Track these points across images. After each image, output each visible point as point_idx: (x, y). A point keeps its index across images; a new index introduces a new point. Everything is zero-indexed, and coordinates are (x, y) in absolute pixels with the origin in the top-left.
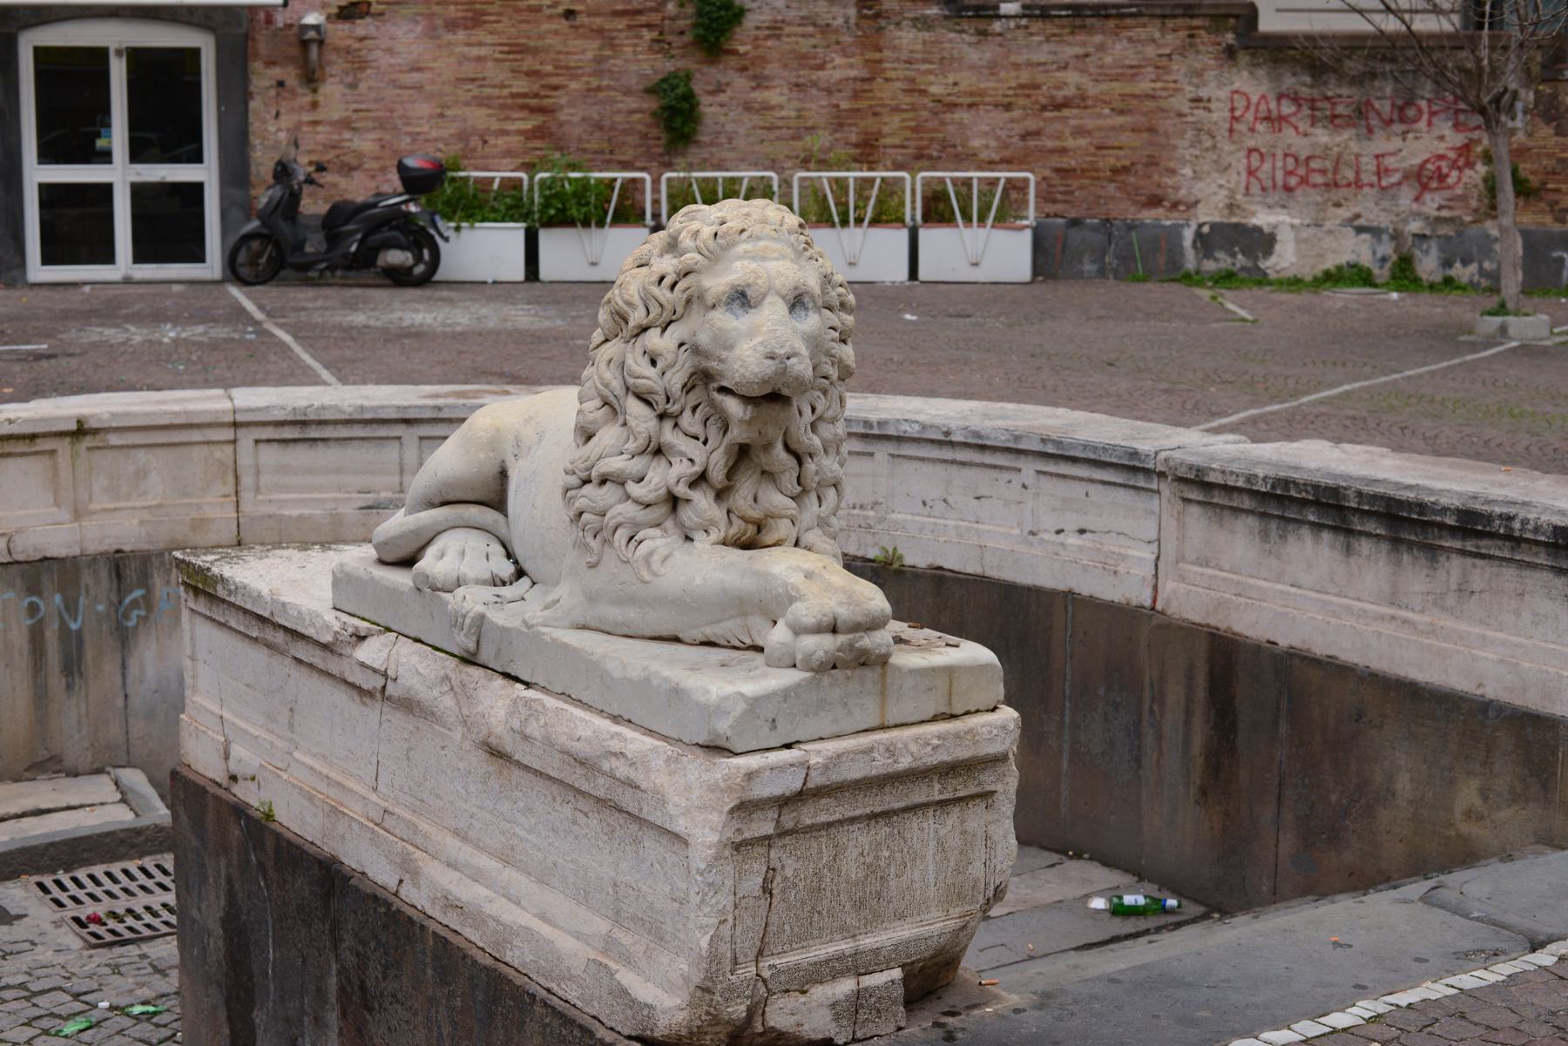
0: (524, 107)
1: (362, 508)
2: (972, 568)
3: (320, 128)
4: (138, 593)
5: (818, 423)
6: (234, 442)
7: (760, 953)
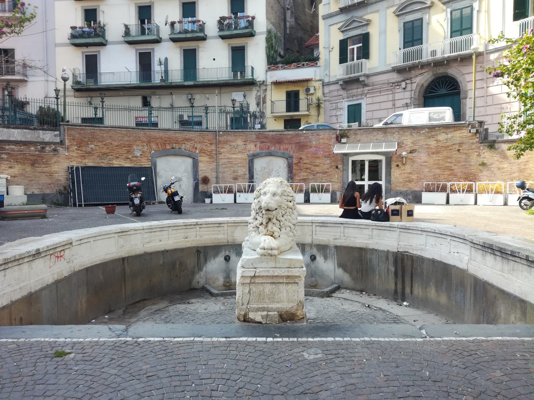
0: (448, 169)
2: (439, 259)
7: (248, 304)
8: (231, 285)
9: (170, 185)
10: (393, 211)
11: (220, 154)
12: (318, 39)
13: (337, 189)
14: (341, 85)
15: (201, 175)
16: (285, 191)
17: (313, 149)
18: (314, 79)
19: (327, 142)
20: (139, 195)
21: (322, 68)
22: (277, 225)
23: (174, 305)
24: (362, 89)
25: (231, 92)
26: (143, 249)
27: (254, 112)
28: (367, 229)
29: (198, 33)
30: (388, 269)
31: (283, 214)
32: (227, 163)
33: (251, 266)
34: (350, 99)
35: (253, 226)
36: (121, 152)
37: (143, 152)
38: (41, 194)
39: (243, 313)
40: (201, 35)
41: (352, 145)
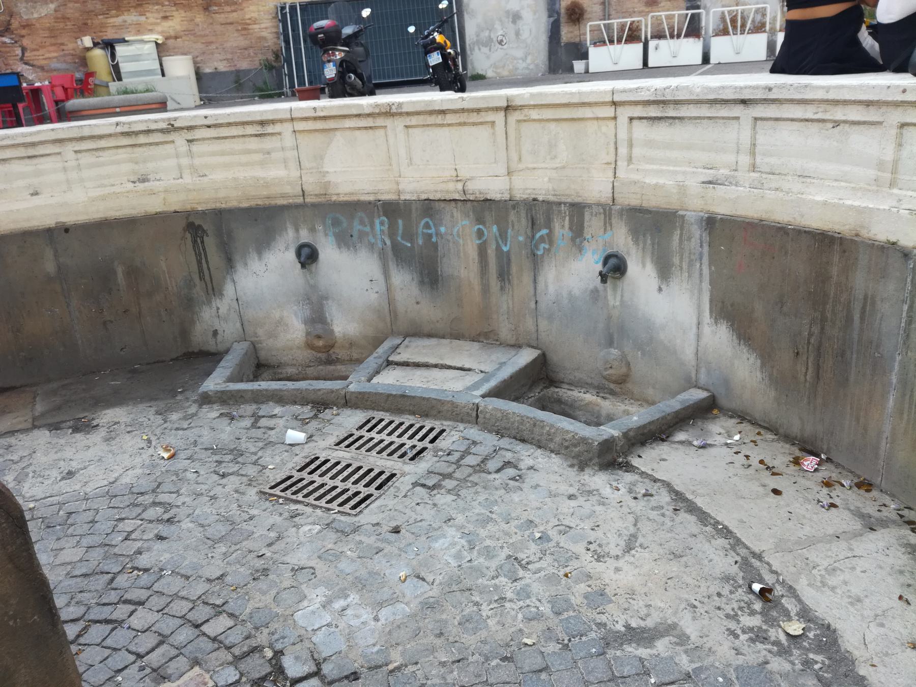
1: (703, 183)
4: (544, 232)
6: (615, 118)
8: (332, 346)
20: (339, 56)
38: (232, 72)
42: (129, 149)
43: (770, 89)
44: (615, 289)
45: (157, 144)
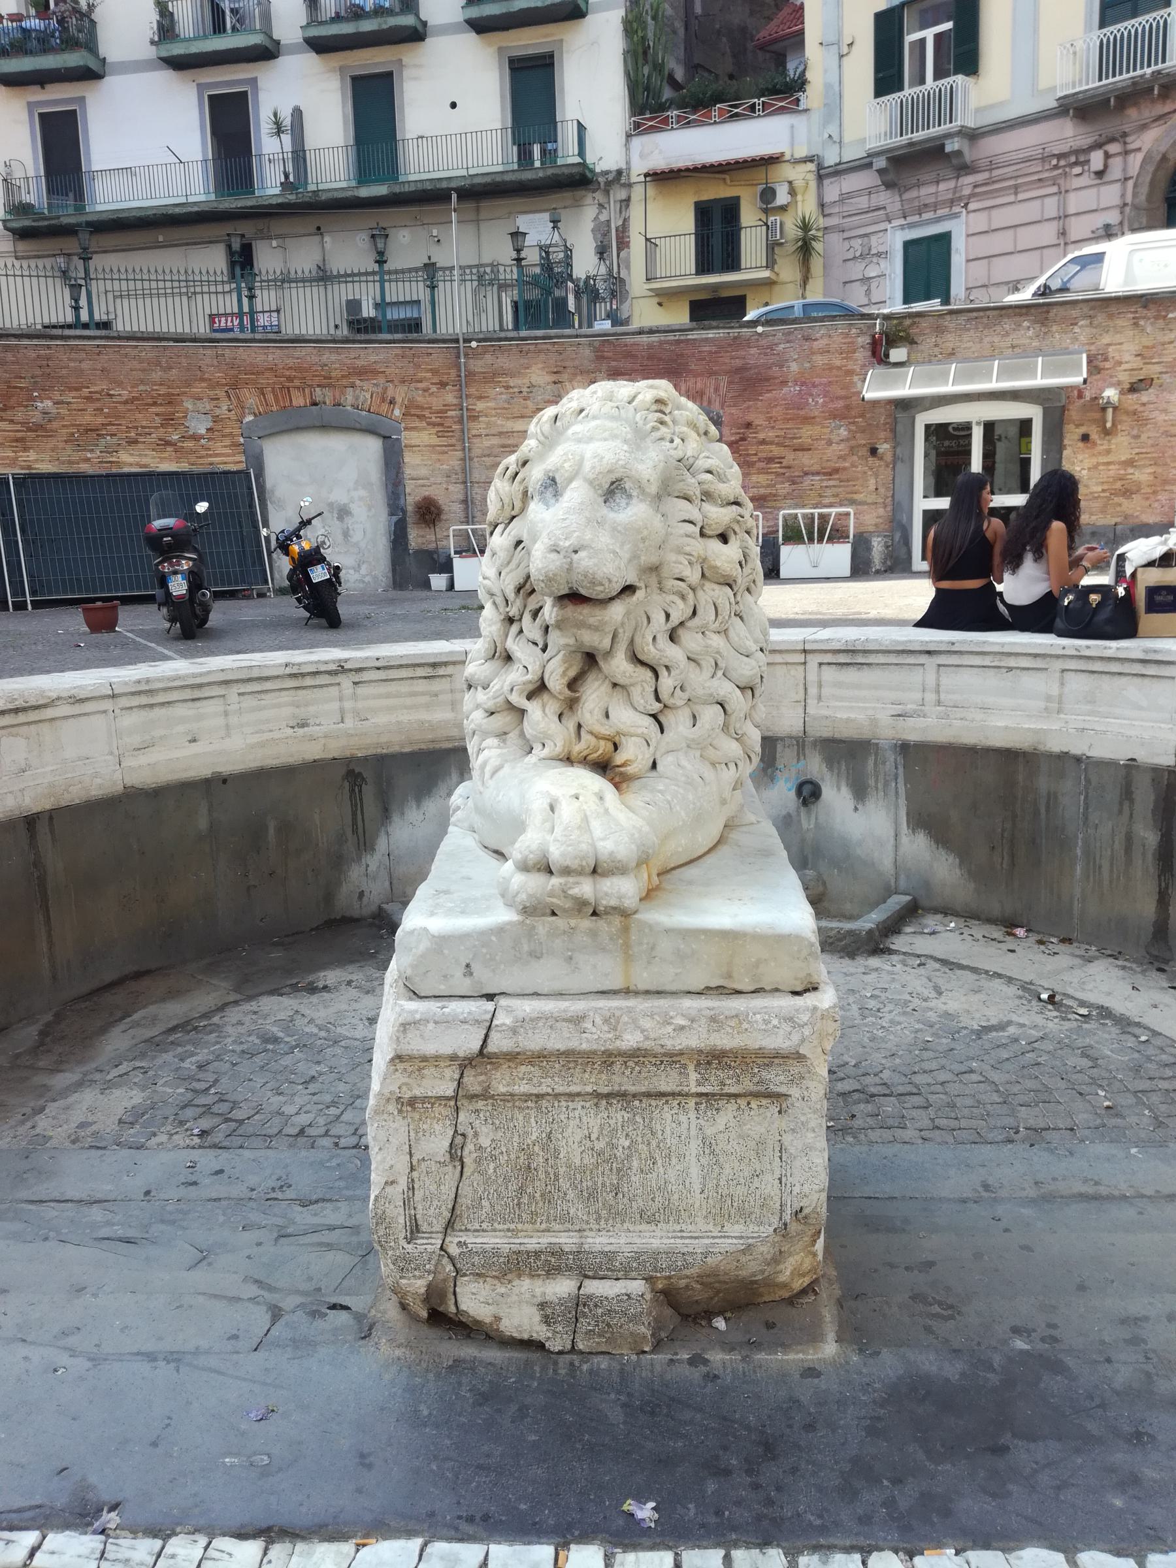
3: (1111, 467)
5: (681, 632)
6: (805, 663)
7: (449, 1226)
9: (299, 529)
10: (1152, 591)
11: (474, 418)
12: (802, 16)
13: (871, 529)
14: (880, 172)
15: (413, 494)
16: (686, 464)
17: (792, 390)
18: (787, 157)
19: (838, 363)
20: (185, 565)
21: (816, 117)
22: (636, 692)
23: (250, 998)
24: (951, 184)
25: (511, 215)
26: (118, 776)
27: (588, 278)
28: (1039, 674)
29: (397, 14)
30: (1129, 839)
31: (675, 619)
32: (497, 450)
33: (463, 985)
34: (910, 219)
35: (490, 705)
36: (144, 423)
37: (216, 419)
39: (418, 1285)
40: (408, 20)
41: (927, 368)
42: (292, 692)
43: (953, 644)
44: (809, 813)
45: (321, 686)
